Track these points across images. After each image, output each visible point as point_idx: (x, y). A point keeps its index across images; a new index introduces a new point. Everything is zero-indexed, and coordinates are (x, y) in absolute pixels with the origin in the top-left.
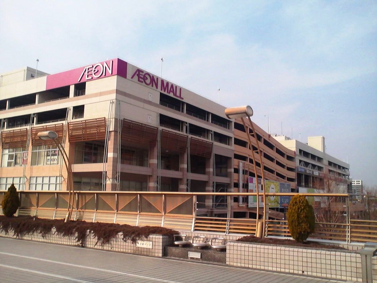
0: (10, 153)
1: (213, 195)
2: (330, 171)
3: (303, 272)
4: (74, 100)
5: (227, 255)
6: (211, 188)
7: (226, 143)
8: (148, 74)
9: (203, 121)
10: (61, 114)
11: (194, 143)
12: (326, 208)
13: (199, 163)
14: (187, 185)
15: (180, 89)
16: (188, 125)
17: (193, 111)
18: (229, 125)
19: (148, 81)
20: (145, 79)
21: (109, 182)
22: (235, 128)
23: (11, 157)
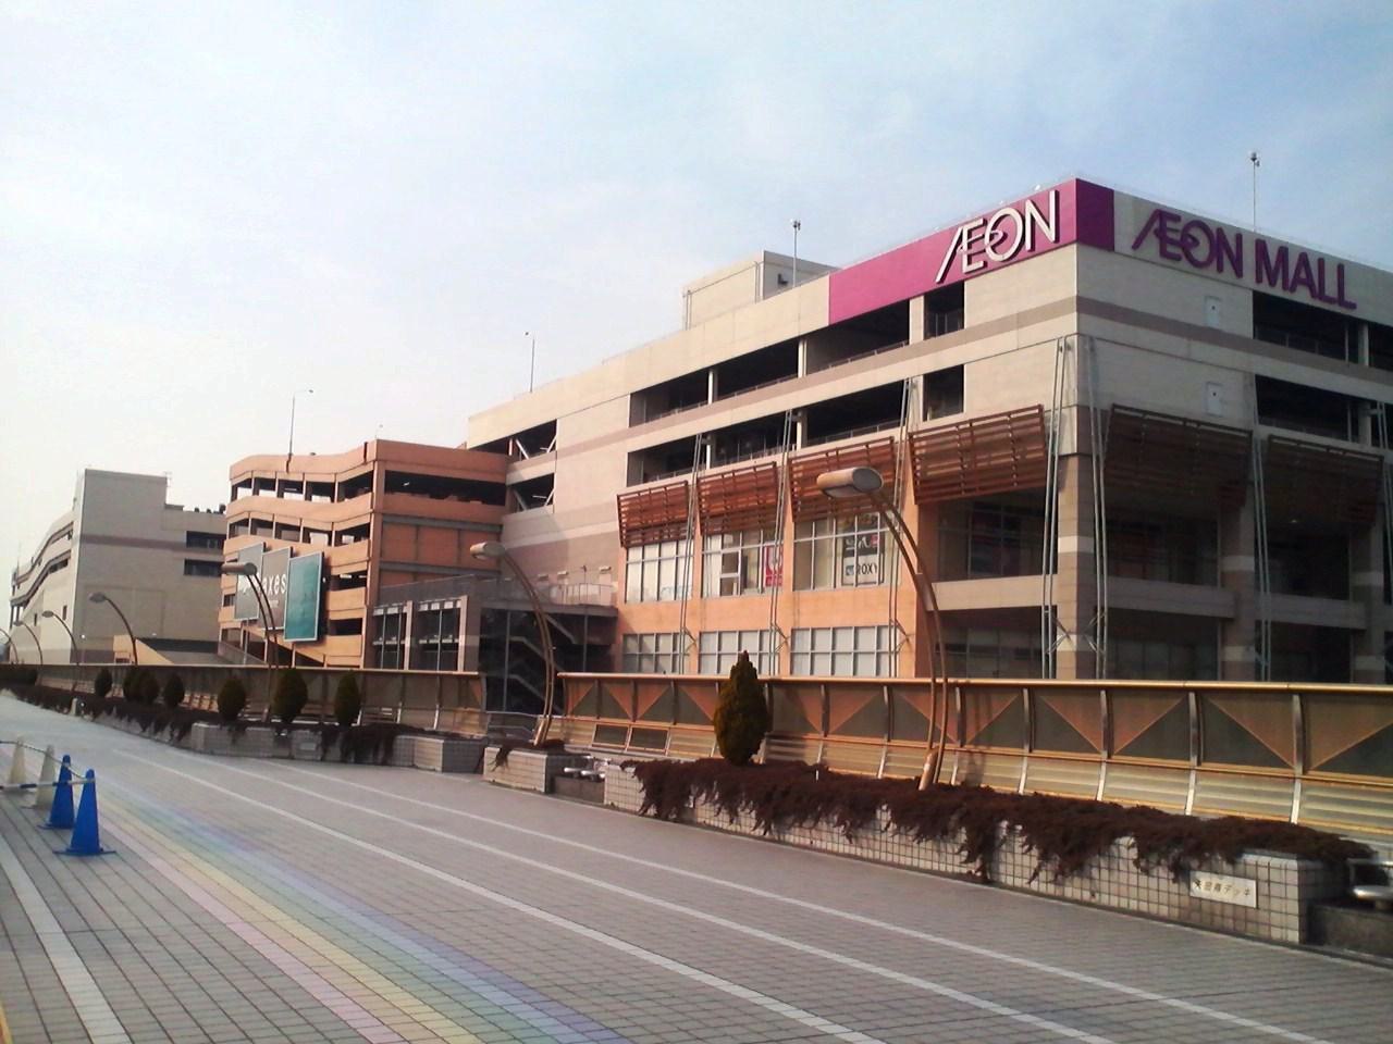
0: (728, 551)
10: (883, 405)
14: (1258, 650)
19: (1202, 252)
20: (1186, 244)
21: (1067, 646)
23: (729, 562)
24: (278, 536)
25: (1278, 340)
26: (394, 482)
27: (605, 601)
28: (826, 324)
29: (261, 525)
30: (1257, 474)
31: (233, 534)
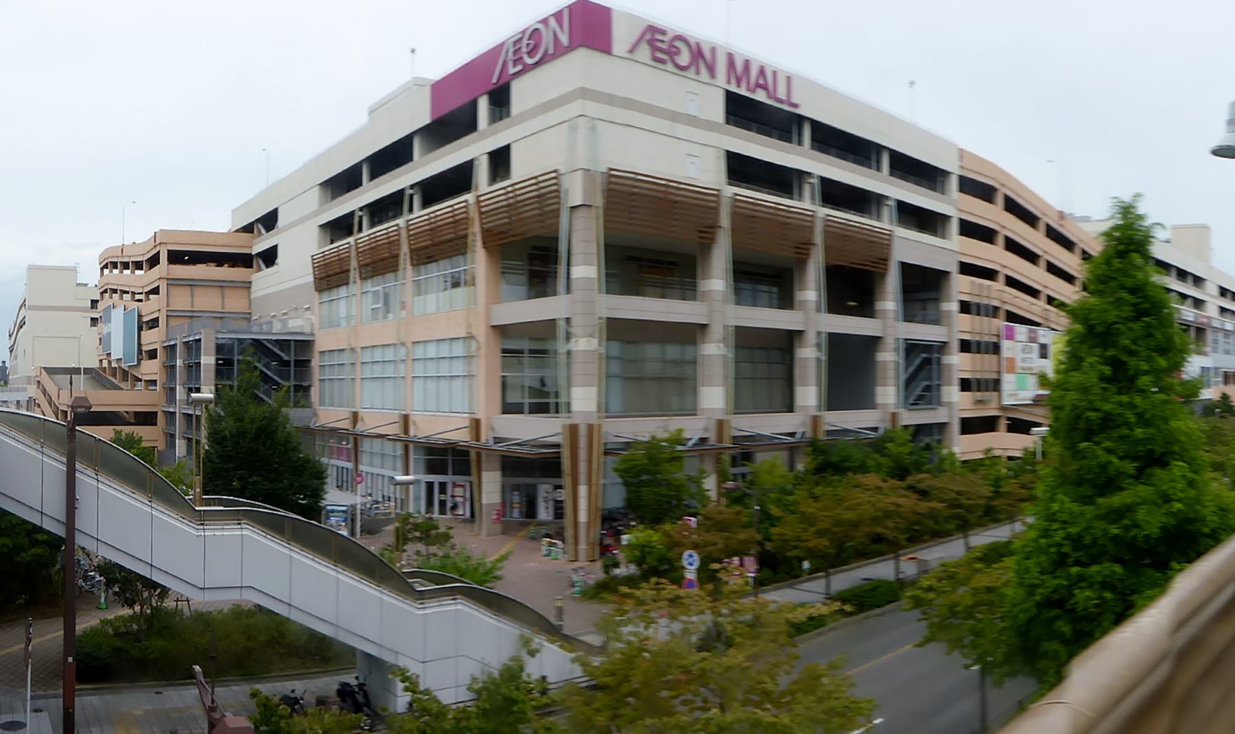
2: (1223, 310)
4: (494, 134)
8: (680, 38)
11: (835, 235)
12: (437, 528)
15: (789, 79)
16: (815, 181)
17: (831, 140)
19: (684, 59)
20: (672, 52)
26: (176, 257)
27: (307, 330)
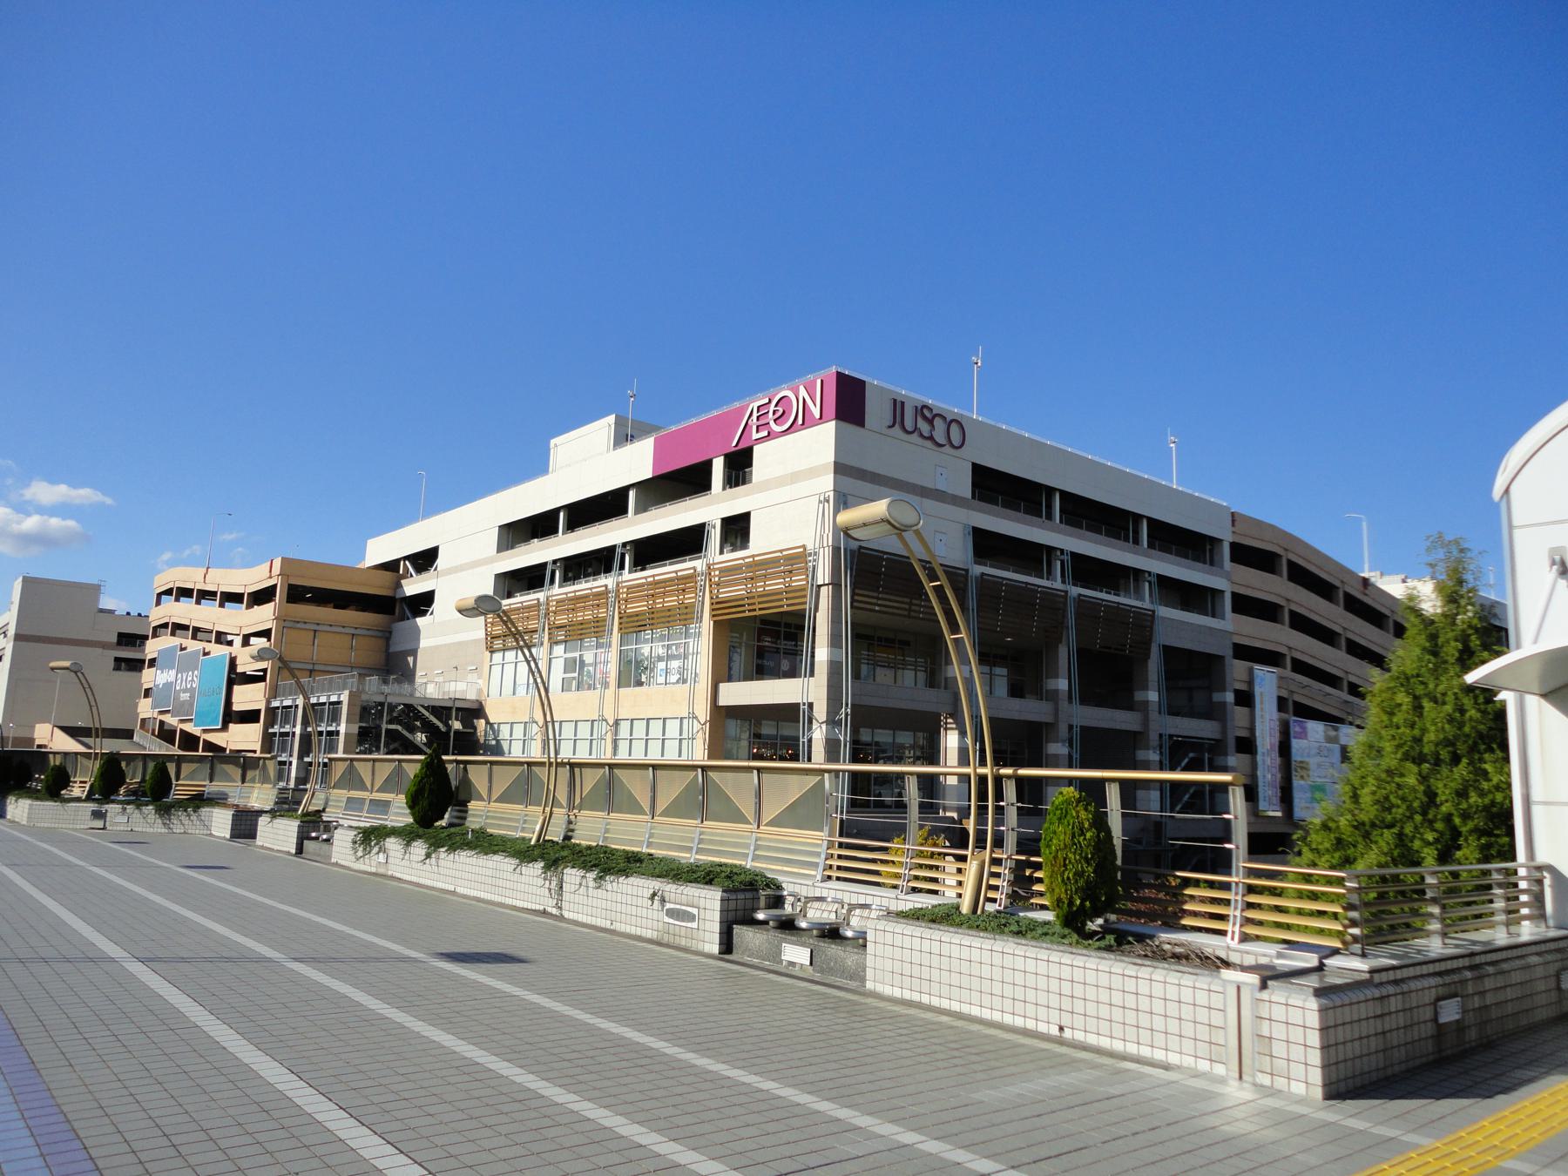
0: (569, 655)
1: (1162, 782)
3: (1061, 1029)
4: (969, 507)
5: (870, 961)
6: (1154, 756)
7: (1203, 612)
9: (1121, 543)
10: (688, 542)
13: (1108, 674)
14: (1071, 745)
18: (1211, 551)
21: (819, 734)
22: (1232, 560)
23: (569, 665)
24: (194, 637)
25: (991, 500)
26: (296, 594)
27: (471, 696)
28: (649, 475)
29: (178, 628)
30: (1071, 620)
31: (155, 635)
